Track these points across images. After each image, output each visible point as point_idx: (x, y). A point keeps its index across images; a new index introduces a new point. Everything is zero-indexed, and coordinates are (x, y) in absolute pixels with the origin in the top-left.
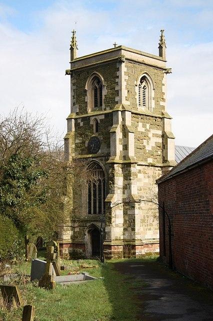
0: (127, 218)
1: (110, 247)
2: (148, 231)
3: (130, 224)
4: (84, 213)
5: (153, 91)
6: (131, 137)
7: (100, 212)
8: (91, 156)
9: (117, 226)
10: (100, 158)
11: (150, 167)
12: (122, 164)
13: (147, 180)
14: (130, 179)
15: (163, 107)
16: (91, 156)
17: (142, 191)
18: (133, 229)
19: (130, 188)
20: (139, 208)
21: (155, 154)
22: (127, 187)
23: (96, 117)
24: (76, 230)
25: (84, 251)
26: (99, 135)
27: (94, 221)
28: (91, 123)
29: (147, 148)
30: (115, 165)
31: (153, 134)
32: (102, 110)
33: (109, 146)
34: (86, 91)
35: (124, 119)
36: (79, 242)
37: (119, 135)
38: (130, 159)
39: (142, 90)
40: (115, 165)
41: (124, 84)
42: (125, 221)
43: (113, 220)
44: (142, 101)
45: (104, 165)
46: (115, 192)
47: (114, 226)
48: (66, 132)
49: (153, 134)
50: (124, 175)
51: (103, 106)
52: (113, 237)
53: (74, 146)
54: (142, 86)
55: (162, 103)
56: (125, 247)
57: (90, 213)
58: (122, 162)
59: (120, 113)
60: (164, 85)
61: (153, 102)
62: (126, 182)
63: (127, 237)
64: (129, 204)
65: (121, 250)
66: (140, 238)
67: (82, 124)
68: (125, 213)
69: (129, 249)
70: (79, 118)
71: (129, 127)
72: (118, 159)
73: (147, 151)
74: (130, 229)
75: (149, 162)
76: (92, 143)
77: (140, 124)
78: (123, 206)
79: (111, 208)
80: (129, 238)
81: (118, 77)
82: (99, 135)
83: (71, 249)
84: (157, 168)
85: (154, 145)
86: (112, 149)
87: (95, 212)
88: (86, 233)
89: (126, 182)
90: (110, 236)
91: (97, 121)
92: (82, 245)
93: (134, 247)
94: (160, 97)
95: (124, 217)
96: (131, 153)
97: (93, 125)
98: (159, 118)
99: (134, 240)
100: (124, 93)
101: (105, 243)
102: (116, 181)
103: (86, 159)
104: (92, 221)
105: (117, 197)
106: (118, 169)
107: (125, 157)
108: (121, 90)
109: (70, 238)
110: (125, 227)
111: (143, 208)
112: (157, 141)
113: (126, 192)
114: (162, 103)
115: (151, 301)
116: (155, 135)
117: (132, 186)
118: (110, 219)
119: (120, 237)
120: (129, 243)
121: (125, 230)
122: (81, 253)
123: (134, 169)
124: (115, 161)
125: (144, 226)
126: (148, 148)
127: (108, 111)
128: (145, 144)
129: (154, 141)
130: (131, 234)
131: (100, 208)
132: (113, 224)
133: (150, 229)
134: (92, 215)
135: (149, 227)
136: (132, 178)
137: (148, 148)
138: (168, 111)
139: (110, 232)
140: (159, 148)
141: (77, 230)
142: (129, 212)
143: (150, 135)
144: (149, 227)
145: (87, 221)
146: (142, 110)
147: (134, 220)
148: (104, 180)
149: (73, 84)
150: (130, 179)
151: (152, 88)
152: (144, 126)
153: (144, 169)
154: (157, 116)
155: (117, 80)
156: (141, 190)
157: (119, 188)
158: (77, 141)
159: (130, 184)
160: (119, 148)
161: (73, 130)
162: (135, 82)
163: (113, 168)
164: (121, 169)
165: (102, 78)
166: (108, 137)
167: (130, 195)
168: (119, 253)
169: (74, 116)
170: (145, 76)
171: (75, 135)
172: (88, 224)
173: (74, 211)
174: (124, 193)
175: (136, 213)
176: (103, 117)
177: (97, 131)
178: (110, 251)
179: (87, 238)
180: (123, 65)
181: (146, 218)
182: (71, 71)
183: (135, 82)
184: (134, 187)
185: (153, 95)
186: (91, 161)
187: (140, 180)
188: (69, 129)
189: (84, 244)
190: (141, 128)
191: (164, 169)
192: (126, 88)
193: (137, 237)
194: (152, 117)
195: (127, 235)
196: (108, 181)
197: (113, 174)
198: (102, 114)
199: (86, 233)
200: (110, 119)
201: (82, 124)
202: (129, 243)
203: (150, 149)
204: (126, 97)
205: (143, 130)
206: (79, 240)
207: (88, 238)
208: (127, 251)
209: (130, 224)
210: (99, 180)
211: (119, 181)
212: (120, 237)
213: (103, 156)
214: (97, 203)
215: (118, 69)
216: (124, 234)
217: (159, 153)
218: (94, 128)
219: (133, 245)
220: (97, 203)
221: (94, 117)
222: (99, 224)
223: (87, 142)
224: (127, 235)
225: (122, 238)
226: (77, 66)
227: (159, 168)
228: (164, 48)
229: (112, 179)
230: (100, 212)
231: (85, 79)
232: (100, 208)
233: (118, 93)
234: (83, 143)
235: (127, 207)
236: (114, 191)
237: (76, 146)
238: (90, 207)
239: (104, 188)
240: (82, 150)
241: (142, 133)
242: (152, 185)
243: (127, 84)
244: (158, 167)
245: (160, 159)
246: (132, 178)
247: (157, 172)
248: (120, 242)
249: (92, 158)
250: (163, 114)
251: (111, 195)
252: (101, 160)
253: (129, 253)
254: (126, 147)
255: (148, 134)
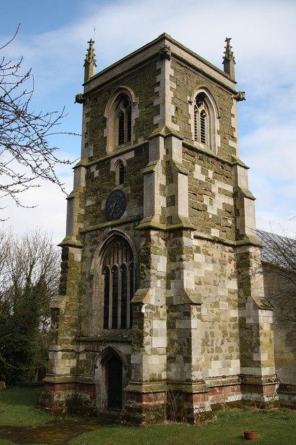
0: (175, 337)
1: (138, 396)
2: (213, 362)
3: (180, 348)
4: (95, 328)
5: (217, 122)
6: (183, 181)
7: (124, 326)
8: (109, 223)
9: (155, 352)
10: (125, 226)
11: (216, 245)
12: (165, 231)
13: (210, 268)
14: (181, 260)
15: (234, 150)
16: (109, 223)
17: (203, 286)
18: (188, 359)
19: (181, 278)
20: (199, 317)
21: (223, 223)
22: (174, 275)
23: (121, 158)
24: (81, 358)
25: (93, 397)
26: (125, 186)
27: (112, 342)
28: (113, 168)
29: (209, 211)
30: (153, 233)
31: (219, 188)
32: (130, 145)
33: (141, 203)
34: (105, 120)
35: (169, 151)
36: (86, 380)
37: (160, 179)
38: (181, 222)
39: (199, 116)
40: (153, 233)
41: (169, 95)
42: (171, 342)
43: (146, 339)
44: (199, 134)
45: (132, 238)
46: (152, 283)
47: (149, 353)
48: (63, 236)
49: (219, 188)
50: (168, 252)
51: (133, 138)
52: (146, 376)
53: (83, 211)
54: (200, 110)
55: (231, 143)
56: (171, 395)
57: (106, 326)
58: (164, 227)
59: (161, 140)
60: (233, 115)
61: (218, 138)
62: (174, 266)
63: (174, 373)
64: (180, 309)
65: (162, 402)
66: (200, 378)
67: (96, 174)
68: (170, 326)
69: (178, 401)
70: (93, 165)
71: (180, 165)
72: (156, 221)
73: (210, 217)
74: (180, 358)
75: (213, 235)
76: (111, 202)
77: (198, 168)
78: (168, 312)
79: (142, 315)
80: (179, 377)
81: (159, 83)
82: (125, 186)
83: (70, 394)
84: (227, 248)
85: (221, 207)
86: (146, 204)
87: (115, 326)
88: (98, 364)
89: (174, 266)
90: (139, 373)
91: (122, 165)
92: (90, 386)
93: (189, 396)
94: (228, 133)
95: (168, 334)
96: (183, 211)
97: (114, 173)
98: (229, 164)
99: (189, 382)
100: (170, 110)
101: (130, 388)
102: (153, 263)
103: (102, 229)
104: (108, 342)
105: (155, 296)
106: (157, 240)
107: (172, 217)
108: (164, 103)
109: (69, 372)
110: (172, 353)
111: (205, 318)
112: (227, 202)
113: (172, 284)
114: (231, 143)
115: (232, 243)
116: (222, 191)
117: (185, 272)
118: (141, 337)
119: (160, 376)
120: (178, 387)
121: (170, 359)
122: (87, 402)
123: (189, 241)
124: (152, 224)
125: (206, 351)
126: (212, 211)
127: (141, 142)
128: (206, 202)
129: (218, 203)
130: (182, 368)
131: (124, 317)
132: (147, 348)
133: (217, 359)
134: (109, 331)
135: (215, 354)
136: (184, 256)
137: (212, 211)
138: (241, 157)
139: (140, 365)
140: (229, 215)
141: (83, 357)
142: (178, 325)
143: (215, 190)
144: (215, 354)
145: (99, 342)
146: (199, 145)
147: (189, 341)
148: (131, 266)
149: (86, 115)
150: (181, 260)
151: (216, 115)
152: (204, 172)
153: (205, 246)
154: (225, 160)
155: (156, 90)
156: (200, 284)
157: (159, 277)
158: (89, 203)
159: (180, 269)
160: (160, 202)
161: (83, 184)
162: (188, 98)
163: (149, 239)
164: (163, 242)
165: (132, 93)
166: (139, 191)
167: (181, 291)
168: (157, 408)
169: (86, 163)
170: (203, 93)
171: (86, 193)
172: (102, 348)
173: (78, 324)
174: (168, 287)
175: (193, 326)
176: (131, 155)
177: (121, 182)
178: (139, 404)
179: (100, 373)
180: (168, 64)
181: (210, 338)
182: (84, 96)
183: (188, 98)
184: (188, 274)
185: (217, 127)
186: (110, 233)
187: (198, 265)
188: (76, 183)
189: (94, 385)
190: (198, 174)
191: (238, 251)
192: (173, 102)
193: (197, 375)
194: (218, 160)
195: (174, 370)
196: (138, 266)
197: (148, 249)
198: (131, 150)
199: (98, 364)
200: (144, 154)
201: (96, 174)
202: (178, 387)
203: (216, 213)
204: (173, 117)
205: (203, 178)
206: (86, 376)
207: (100, 374)
208: (174, 403)
209: (180, 348)
210: (123, 266)
211: (160, 264)
212: (160, 376)
213: (130, 222)
214: (120, 309)
215: (159, 72)
216: (168, 369)
217: (230, 222)
218: (117, 177)
219: (188, 393)
220: (120, 309)
221: (117, 158)
222: (123, 349)
223: (104, 202)
224: (174, 370)
225: (164, 376)
226: (93, 86)
227: (231, 248)
228: (231, 62)
229: (146, 259)
230: (124, 326)
231: (105, 102)
232: (124, 317)
233: (158, 110)
234: (99, 203)
235: (174, 314)
236: (149, 281)
237: (86, 211)
238: (106, 318)
239: (132, 276)
240: (96, 217)
241: (201, 182)
242: (220, 277)
243: (175, 96)
244: (228, 245)
245: (230, 232)
246: (184, 256)
247: (228, 254)
248: (162, 384)
249: (112, 226)
250: (233, 159)
251: (144, 290)
252: (128, 229)
253: (180, 408)
254: (172, 201)
255: (211, 186)
